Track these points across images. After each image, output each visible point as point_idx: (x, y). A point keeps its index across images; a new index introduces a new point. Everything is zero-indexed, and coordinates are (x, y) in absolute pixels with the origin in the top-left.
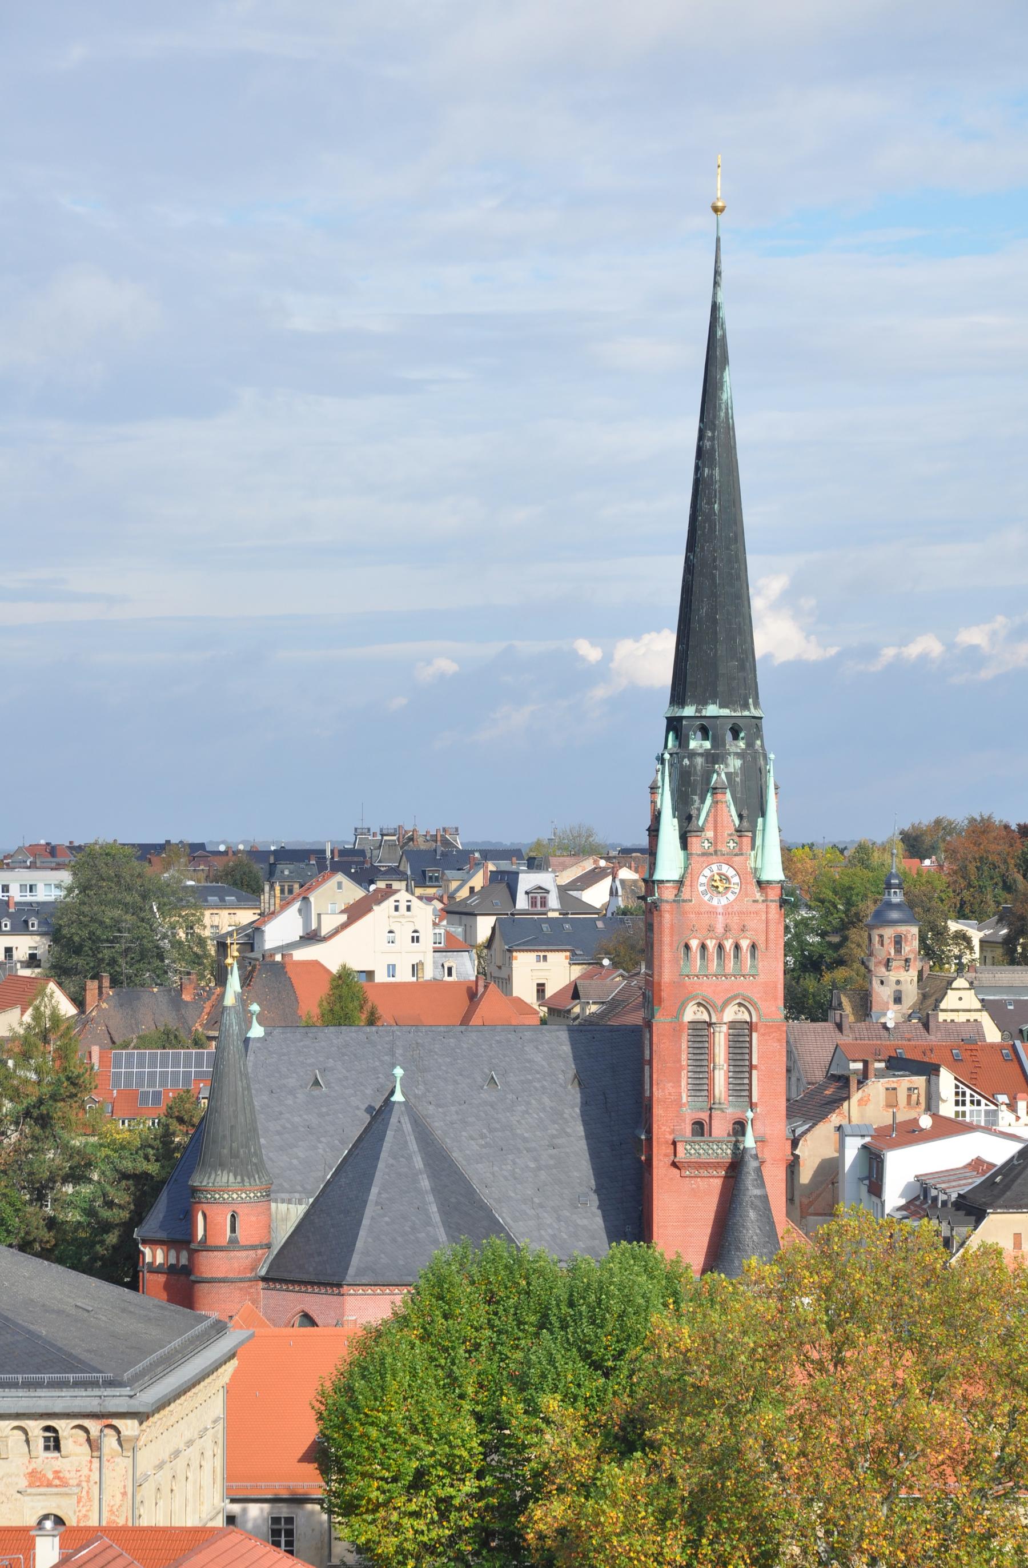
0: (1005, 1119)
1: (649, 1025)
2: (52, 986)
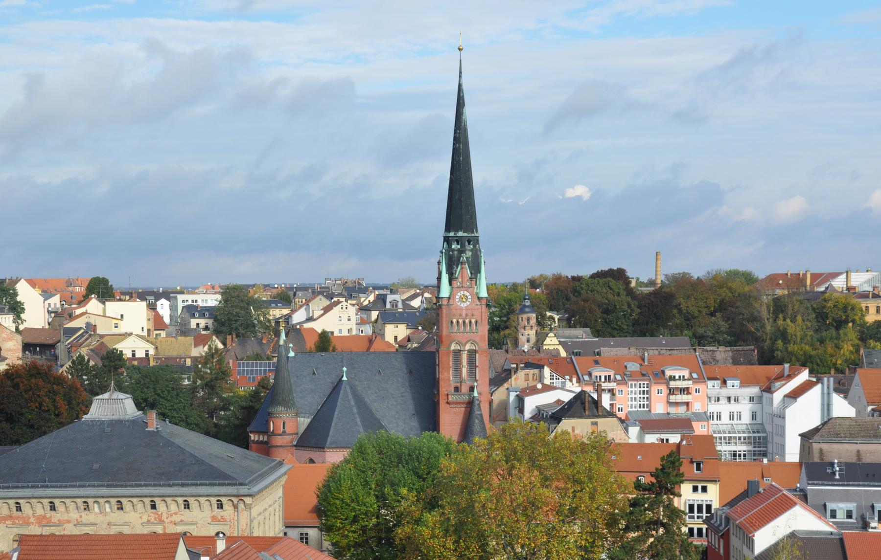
0: (568, 385)
1: (438, 351)
2: (214, 338)
